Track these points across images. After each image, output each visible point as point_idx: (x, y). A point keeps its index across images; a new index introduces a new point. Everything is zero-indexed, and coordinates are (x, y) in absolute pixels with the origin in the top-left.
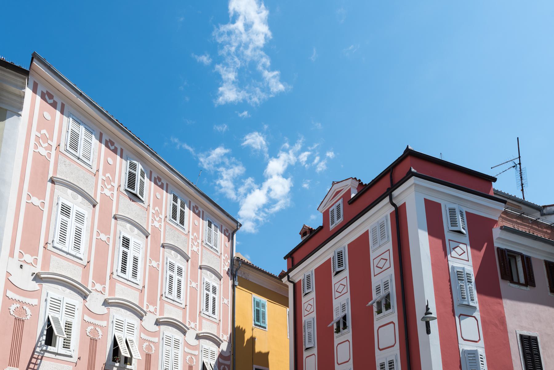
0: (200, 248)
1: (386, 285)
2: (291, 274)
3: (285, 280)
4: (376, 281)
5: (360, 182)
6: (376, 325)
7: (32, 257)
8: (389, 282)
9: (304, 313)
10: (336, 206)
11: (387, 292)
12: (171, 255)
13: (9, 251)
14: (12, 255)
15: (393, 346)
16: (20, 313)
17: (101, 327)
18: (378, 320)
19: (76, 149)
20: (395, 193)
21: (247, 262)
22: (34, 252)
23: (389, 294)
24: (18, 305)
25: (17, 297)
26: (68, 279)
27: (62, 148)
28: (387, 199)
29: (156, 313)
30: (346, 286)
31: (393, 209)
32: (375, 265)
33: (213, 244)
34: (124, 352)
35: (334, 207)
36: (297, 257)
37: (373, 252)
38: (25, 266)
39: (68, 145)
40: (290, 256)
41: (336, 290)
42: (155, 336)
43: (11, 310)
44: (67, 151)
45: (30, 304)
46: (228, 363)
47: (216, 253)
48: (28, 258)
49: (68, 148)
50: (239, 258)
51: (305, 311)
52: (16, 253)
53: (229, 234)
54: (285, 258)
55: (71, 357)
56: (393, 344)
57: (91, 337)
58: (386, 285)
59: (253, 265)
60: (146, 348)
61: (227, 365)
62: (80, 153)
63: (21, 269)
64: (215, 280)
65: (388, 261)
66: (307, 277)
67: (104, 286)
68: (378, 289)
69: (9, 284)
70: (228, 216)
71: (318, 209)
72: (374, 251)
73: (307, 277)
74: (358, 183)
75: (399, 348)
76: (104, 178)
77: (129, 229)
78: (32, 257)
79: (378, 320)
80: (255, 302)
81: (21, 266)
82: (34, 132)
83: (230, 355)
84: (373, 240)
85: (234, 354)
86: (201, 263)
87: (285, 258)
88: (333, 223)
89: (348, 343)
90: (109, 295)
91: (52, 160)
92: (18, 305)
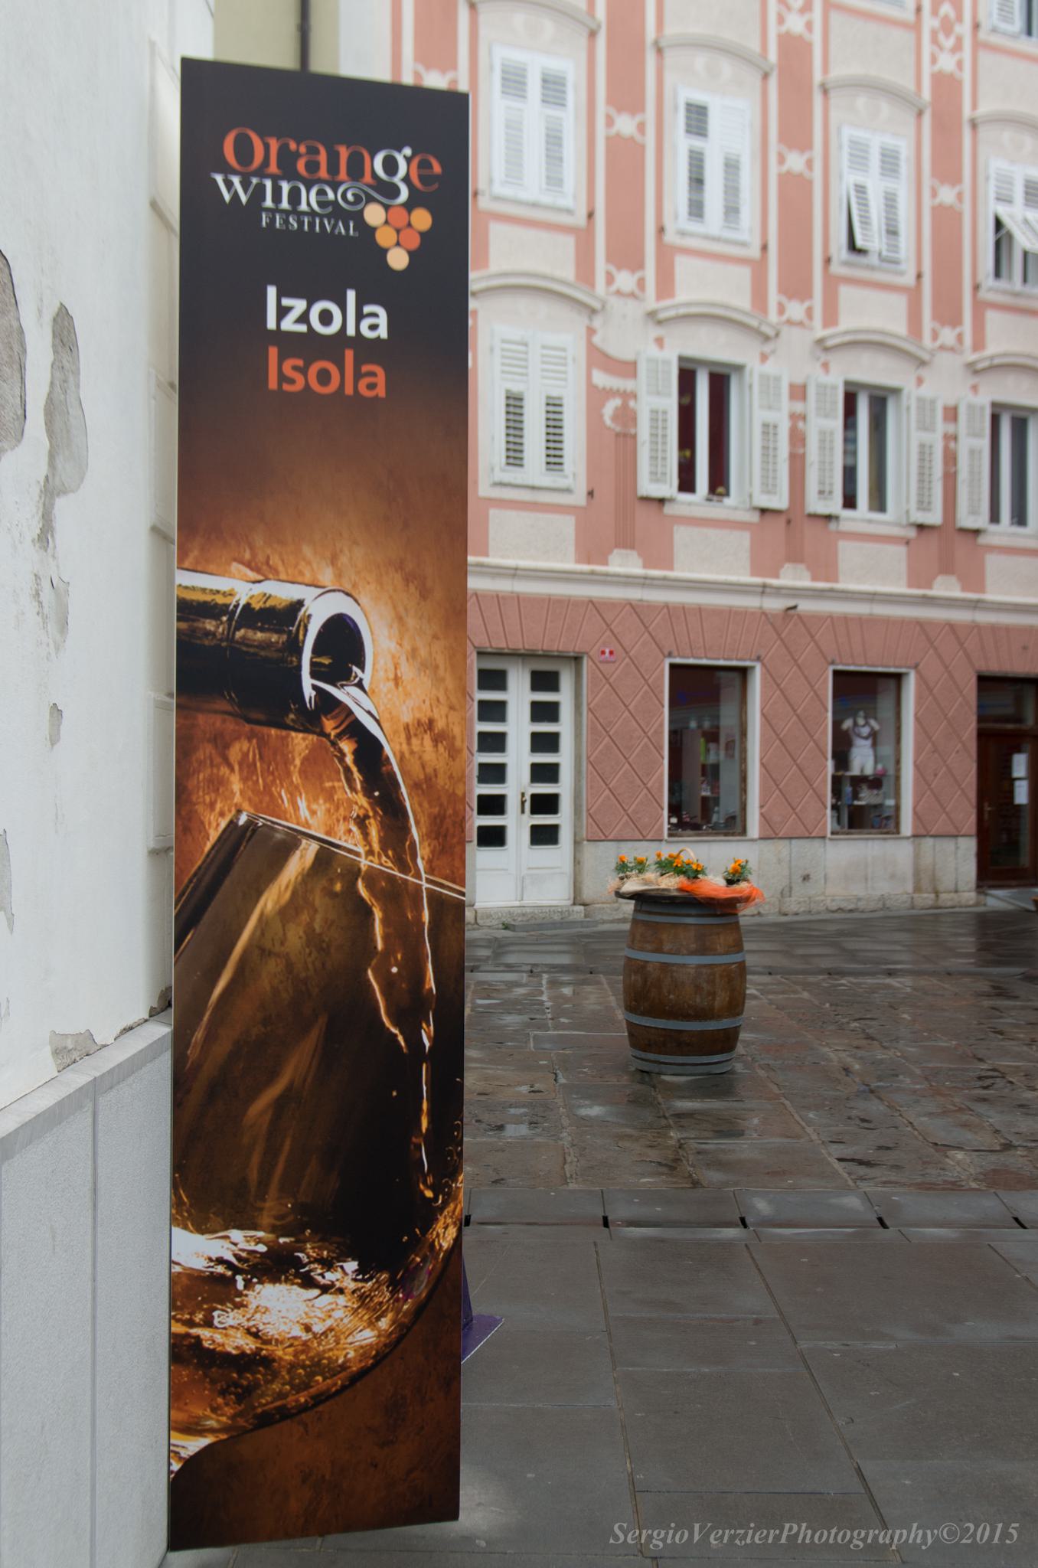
0: (967, 54)
60: (616, 418)
86: (974, 106)
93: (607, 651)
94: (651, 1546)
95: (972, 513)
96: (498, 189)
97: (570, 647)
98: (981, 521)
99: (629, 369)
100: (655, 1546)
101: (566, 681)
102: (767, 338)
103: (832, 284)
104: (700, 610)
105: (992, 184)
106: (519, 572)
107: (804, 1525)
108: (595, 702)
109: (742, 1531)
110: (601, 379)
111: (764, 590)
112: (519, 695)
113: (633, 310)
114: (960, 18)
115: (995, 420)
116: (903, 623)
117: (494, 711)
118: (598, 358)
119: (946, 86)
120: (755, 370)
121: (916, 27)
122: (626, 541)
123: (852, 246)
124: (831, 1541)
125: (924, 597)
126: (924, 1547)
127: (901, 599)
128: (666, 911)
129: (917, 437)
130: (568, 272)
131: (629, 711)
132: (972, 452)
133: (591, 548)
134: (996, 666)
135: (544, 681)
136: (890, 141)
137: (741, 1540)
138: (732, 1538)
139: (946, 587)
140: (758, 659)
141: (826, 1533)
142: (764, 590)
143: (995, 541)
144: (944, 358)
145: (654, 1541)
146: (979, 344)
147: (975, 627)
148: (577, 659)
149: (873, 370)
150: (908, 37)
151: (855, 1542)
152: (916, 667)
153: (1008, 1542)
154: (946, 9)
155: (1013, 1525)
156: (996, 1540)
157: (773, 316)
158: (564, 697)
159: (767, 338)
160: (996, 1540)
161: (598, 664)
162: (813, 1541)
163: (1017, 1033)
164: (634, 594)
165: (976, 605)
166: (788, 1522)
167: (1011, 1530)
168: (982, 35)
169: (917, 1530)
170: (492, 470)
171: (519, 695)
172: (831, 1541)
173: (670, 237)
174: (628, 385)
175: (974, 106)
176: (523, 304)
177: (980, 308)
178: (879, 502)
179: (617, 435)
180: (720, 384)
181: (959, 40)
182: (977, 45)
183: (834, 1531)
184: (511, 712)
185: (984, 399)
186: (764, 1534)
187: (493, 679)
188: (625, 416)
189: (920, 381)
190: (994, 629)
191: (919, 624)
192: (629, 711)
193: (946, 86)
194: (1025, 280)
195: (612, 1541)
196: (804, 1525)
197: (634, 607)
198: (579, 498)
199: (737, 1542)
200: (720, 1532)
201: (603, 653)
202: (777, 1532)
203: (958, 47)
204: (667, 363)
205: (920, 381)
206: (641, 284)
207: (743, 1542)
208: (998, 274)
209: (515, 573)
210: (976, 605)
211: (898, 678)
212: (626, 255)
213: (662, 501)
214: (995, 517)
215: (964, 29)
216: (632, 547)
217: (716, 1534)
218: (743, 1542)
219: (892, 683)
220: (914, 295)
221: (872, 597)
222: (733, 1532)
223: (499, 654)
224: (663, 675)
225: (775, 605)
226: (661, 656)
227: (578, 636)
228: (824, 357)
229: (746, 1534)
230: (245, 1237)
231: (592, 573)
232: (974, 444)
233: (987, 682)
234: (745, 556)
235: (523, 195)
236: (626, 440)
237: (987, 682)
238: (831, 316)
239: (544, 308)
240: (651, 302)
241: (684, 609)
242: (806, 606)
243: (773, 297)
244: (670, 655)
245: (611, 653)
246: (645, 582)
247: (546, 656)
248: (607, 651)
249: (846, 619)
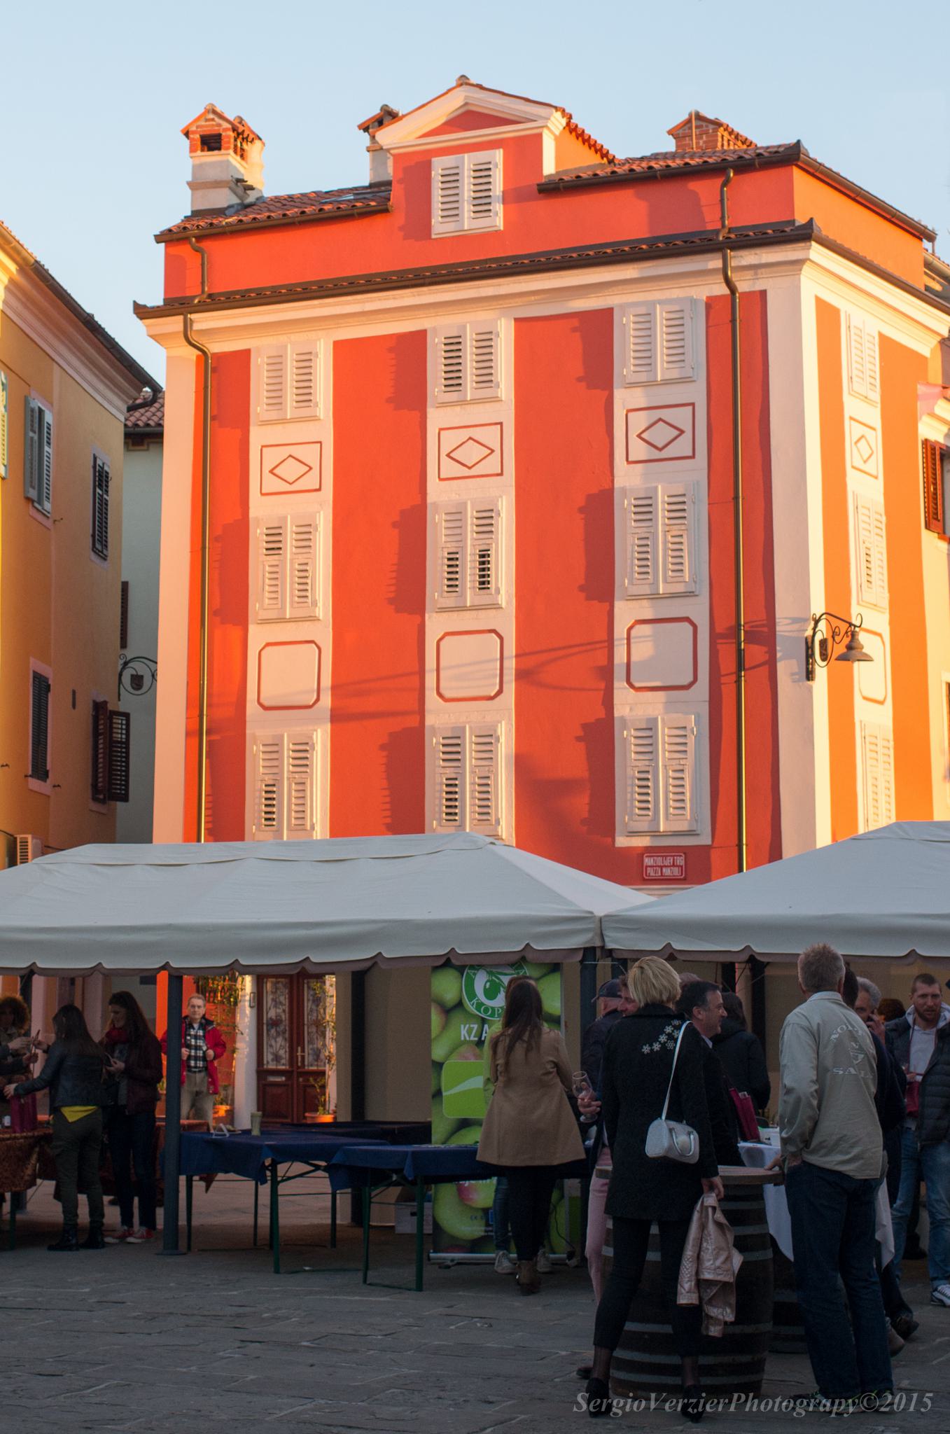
2: (203, 321)
15: (268, 645)
30: (688, 434)
54: (159, 239)
56: (269, 649)
75: (707, 697)
87: (159, 239)
94: (795, 1414)
100: (798, 1414)
107: (751, 1395)
109: (694, 1401)
124: (776, 1409)
126: (845, 1415)
127: (911, 289)
128: (86, 936)
137: (693, 1409)
138: (685, 1407)
141: (771, 1402)
145: (614, 1409)
151: (798, 1410)
153: (923, 1410)
155: (928, 1395)
156: (912, 1409)
160: (912, 1409)
162: (781, 1409)
163: (651, 905)
166: (736, 1392)
167: (925, 1399)
169: (753, 1399)
172: (776, 1409)
183: (778, 1400)
186: (598, 1403)
195: (575, 1409)
196: (751, 1395)
199: (690, 1410)
200: (599, 1401)
202: (727, 1401)
207: (695, 1411)
217: (595, 1403)
218: (695, 1411)
222: (686, 1401)
229: (698, 1402)
230: (770, 1145)
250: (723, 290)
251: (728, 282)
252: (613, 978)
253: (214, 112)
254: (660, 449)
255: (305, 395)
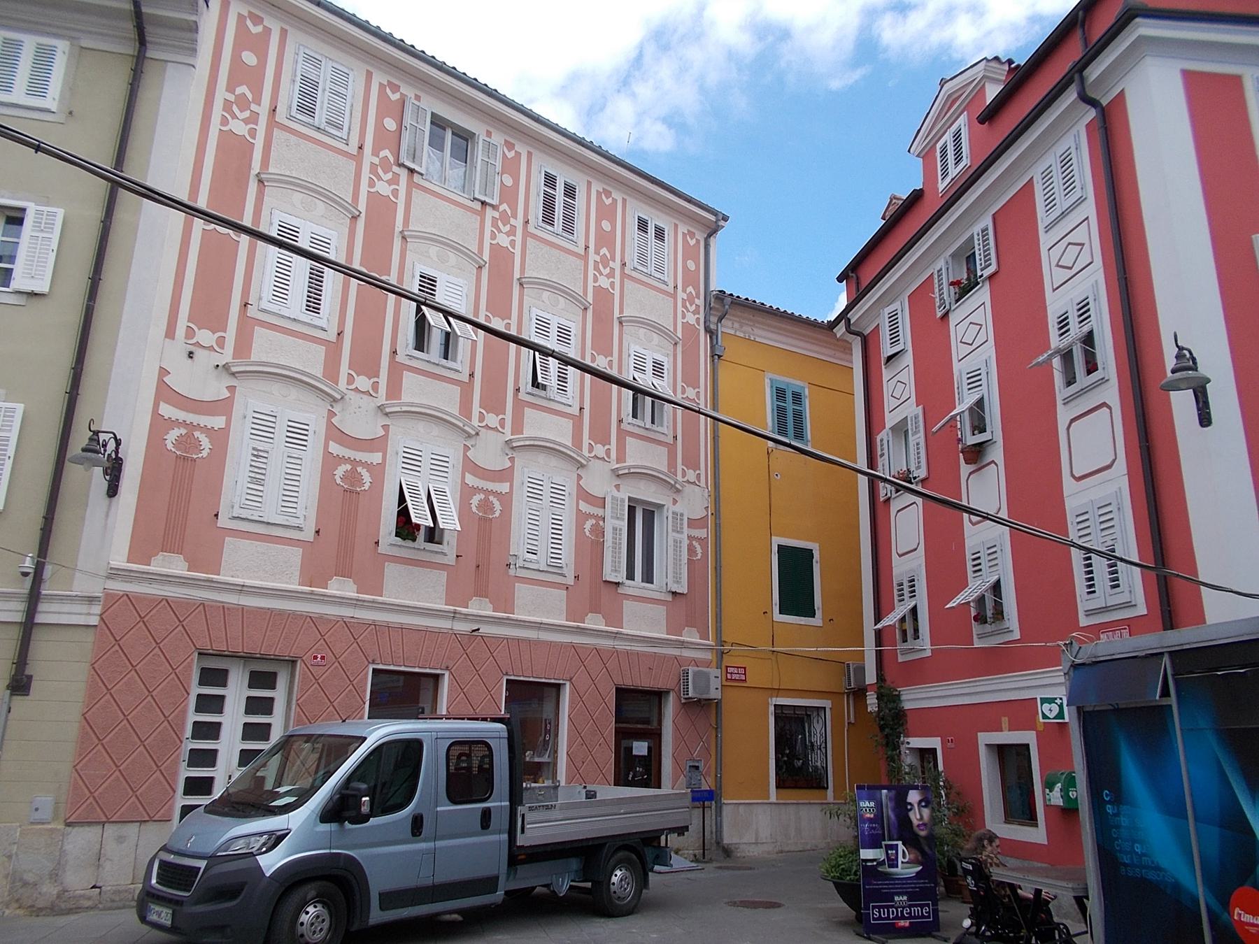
0: (518, 238)
1: (1084, 310)
3: (840, 330)
4: (1057, 303)
5: (1013, 66)
6: (1063, 415)
7: (214, 333)
8: (1091, 300)
9: (889, 403)
10: (952, 135)
11: (1086, 329)
12: (543, 301)
13: (165, 328)
14: (170, 333)
16: (188, 446)
17: (368, 466)
18: (1068, 402)
19: (311, 112)
20: (1094, 72)
21: (747, 299)
22: (218, 324)
23: (1091, 333)
24: (183, 431)
25: (181, 415)
26: (312, 378)
27: (281, 117)
28: (1071, 95)
29: (504, 429)
30: (984, 326)
31: (1092, 113)
32: (1054, 263)
33: (653, 268)
34: (420, 517)
35: (948, 137)
36: (868, 273)
37: (1046, 232)
38: (199, 353)
39: (295, 107)
40: (850, 274)
41: (959, 341)
42: (501, 481)
43: (167, 442)
44: (291, 118)
45: (188, 422)
46: (701, 533)
47: (663, 287)
48: (205, 337)
49: (293, 114)
50: (725, 293)
51: (890, 397)
52: (180, 331)
53: (698, 241)
54: (840, 279)
55: (299, 528)
57: (346, 487)
58: (1084, 310)
59: (763, 304)
60: (479, 507)
61: (699, 540)
62: (320, 117)
63: (190, 360)
64: (659, 346)
65: (1086, 247)
66: (890, 318)
67: (376, 380)
68: (1063, 323)
69: (164, 392)
70: (689, 200)
71: (909, 151)
72: (1048, 229)
73: (890, 318)
74: (1007, 69)
76: (376, 161)
77: (435, 259)
78: (214, 333)
79: (1068, 402)
80: (775, 389)
81: (191, 353)
82: (221, 94)
83: (707, 515)
84: (1046, 200)
85: (717, 514)
86: (621, 311)
87: (840, 279)
88: (945, 174)
89: (995, 467)
90: (388, 397)
91: (259, 143)
92: (183, 431)
93: (319, 656)
95: (614, 570)
96: (265, 305)
97: (287, 653)
98: (621, 576)
99: (602, 502)
101: (282, 682)
102: (469, 436)
103: (396, 370)
104: (402, 628)
105: (632, 361)
106: (245, 589)
108: (301, 700)
110: (471, 480)
111: (455, 616)
112: (236, 692)
113: (368, 404)
114: (258, 101)
115: (632, 510)
116: (562, 645)
117: (212, 704)
118: (583, 495)
119: (603, 295)
120: (670, 508)
121: (585, 258)
122: (595, 609)
123: (535, 383)
125: (578, 627)
129: (672, 535)
130: (318, 371)
131: (333, 706)
132: (615, 529)
133: (314, 573)
134: (628, 682)
135: (262, 679)
136: (660, 357)
139: (594, 622)
140: (447, 668)
142: (455, 616)
143: (630, 591)
144: (596, 464)
146: (621, 458)
147: (615, 652)
148: (294, 662)
149: (648, 493)
150: (580, 263)
152: (570, 680)
154: (690, 289)
157: (475, 422)
158: (279, 695)
159: (469, 436)
161: (310, 667)
164: (347, 612)
165: (616, 636)
168: (627, 271)
170: (233, 507)
171: (236, 692)
173: (400, 358)
174: (599, 512)
175: (621, 311)
176: (421, 426)
177: (622, 434)
178: (648, 577)
179: (480, 518)
180: (649, 517)
181: (613, 270)
182: (623, 275)
184: (228, 705)
185: (624, 495)
187: (213, 676)
188: (599, 531)
189: (675, 502)
190: (628, 653)
191: (573, 646)
192: (333, 706)
193: (603, 295)
194: (653, 422)
197: (347, 624)
198: (309, 535)
201: (315, 658)
203: (611, 275)
204: (622, 500)
205: (675, 502)
206: (375, 386)
208: (635, 416)
209: (242, 589)
210: (375, 606)
211: (558, 687)
212: (493, 403)
213: (618, 584)
214: (630, 576)
215: (617, 265)
216: (180, 552)
219: (554, 690)
220: (577, 420)
221: (539, 626)
223: (220, 655)
224: (366, 678)
225: (463, 627)
226: (367, 663)
227: (294, 644)
228: (387, 421)
231: (312, 593)
232: (616, 524)
233: (623, 694)
234: (442, 589)
235: (286, 313)
236: (598, 546)
237: (623, 694)
238: (518, 427)
239: (554, 462)
240: (382, 400)
241: (388, 626)
242: (486, 630)
243: (680, 467)
244: (373, 662)
245: (323, 658)
246: (357, 603)
247: (263, 658)
248: (319, 656)
249: (519, 640)
250: (1092, 113)
251: (1093, 103)
252: (775, 705)
253: (895, 198)
254: (1070, 268)
255: (1069, 185)
